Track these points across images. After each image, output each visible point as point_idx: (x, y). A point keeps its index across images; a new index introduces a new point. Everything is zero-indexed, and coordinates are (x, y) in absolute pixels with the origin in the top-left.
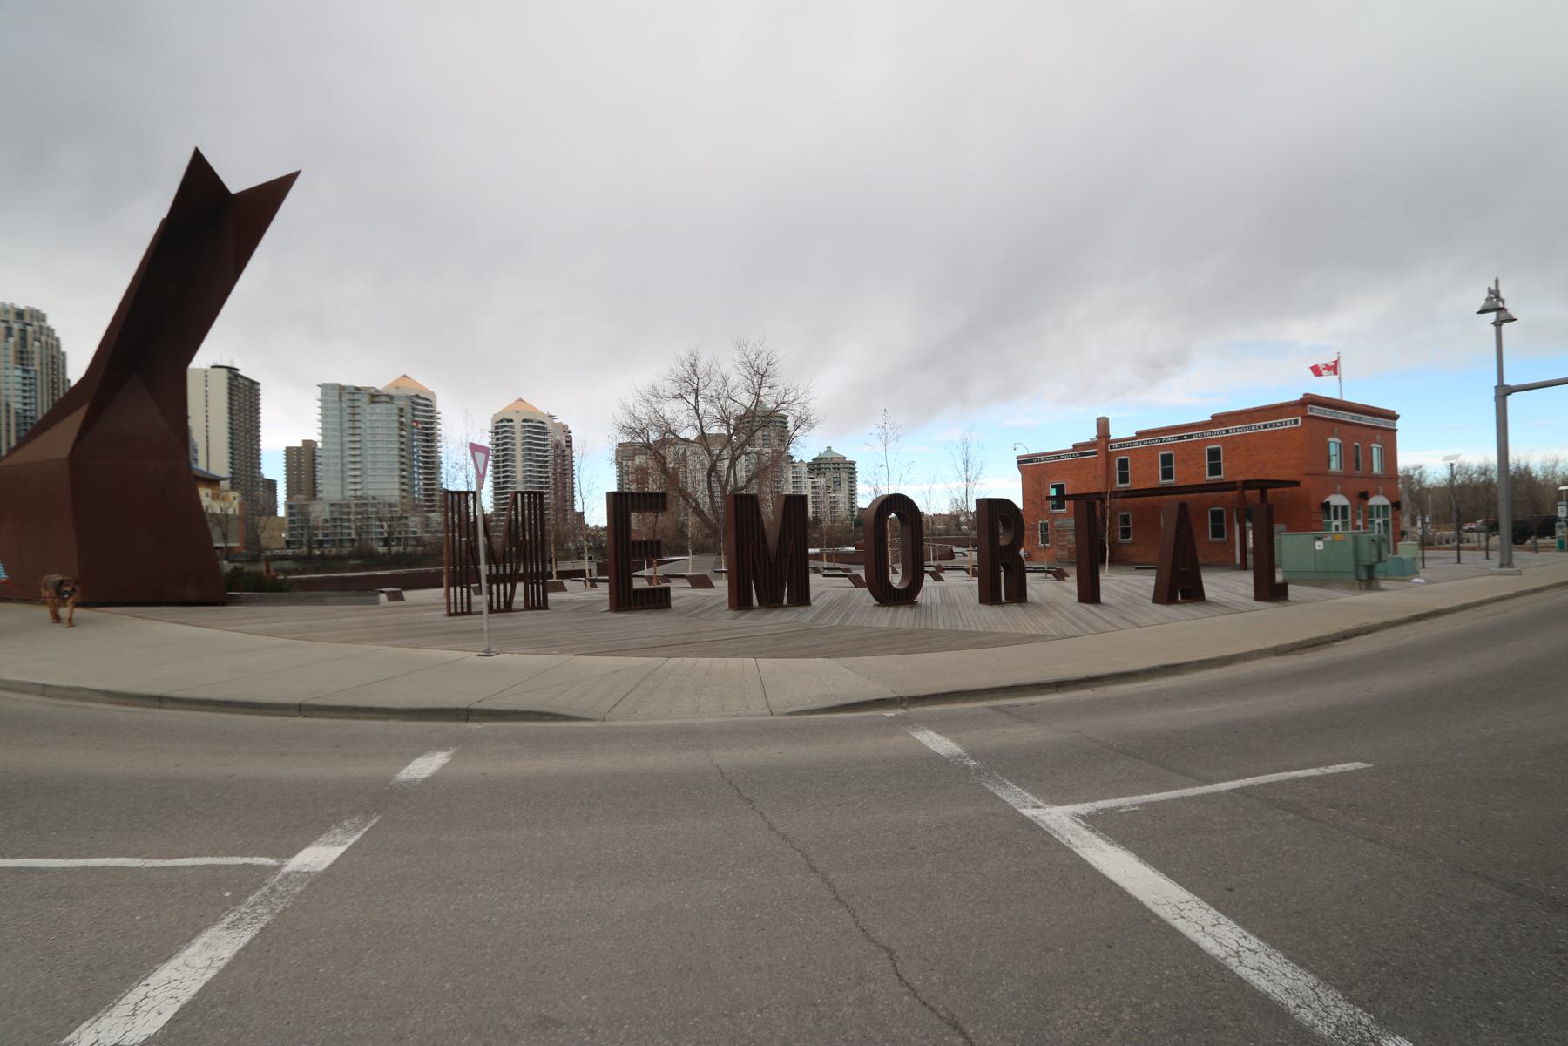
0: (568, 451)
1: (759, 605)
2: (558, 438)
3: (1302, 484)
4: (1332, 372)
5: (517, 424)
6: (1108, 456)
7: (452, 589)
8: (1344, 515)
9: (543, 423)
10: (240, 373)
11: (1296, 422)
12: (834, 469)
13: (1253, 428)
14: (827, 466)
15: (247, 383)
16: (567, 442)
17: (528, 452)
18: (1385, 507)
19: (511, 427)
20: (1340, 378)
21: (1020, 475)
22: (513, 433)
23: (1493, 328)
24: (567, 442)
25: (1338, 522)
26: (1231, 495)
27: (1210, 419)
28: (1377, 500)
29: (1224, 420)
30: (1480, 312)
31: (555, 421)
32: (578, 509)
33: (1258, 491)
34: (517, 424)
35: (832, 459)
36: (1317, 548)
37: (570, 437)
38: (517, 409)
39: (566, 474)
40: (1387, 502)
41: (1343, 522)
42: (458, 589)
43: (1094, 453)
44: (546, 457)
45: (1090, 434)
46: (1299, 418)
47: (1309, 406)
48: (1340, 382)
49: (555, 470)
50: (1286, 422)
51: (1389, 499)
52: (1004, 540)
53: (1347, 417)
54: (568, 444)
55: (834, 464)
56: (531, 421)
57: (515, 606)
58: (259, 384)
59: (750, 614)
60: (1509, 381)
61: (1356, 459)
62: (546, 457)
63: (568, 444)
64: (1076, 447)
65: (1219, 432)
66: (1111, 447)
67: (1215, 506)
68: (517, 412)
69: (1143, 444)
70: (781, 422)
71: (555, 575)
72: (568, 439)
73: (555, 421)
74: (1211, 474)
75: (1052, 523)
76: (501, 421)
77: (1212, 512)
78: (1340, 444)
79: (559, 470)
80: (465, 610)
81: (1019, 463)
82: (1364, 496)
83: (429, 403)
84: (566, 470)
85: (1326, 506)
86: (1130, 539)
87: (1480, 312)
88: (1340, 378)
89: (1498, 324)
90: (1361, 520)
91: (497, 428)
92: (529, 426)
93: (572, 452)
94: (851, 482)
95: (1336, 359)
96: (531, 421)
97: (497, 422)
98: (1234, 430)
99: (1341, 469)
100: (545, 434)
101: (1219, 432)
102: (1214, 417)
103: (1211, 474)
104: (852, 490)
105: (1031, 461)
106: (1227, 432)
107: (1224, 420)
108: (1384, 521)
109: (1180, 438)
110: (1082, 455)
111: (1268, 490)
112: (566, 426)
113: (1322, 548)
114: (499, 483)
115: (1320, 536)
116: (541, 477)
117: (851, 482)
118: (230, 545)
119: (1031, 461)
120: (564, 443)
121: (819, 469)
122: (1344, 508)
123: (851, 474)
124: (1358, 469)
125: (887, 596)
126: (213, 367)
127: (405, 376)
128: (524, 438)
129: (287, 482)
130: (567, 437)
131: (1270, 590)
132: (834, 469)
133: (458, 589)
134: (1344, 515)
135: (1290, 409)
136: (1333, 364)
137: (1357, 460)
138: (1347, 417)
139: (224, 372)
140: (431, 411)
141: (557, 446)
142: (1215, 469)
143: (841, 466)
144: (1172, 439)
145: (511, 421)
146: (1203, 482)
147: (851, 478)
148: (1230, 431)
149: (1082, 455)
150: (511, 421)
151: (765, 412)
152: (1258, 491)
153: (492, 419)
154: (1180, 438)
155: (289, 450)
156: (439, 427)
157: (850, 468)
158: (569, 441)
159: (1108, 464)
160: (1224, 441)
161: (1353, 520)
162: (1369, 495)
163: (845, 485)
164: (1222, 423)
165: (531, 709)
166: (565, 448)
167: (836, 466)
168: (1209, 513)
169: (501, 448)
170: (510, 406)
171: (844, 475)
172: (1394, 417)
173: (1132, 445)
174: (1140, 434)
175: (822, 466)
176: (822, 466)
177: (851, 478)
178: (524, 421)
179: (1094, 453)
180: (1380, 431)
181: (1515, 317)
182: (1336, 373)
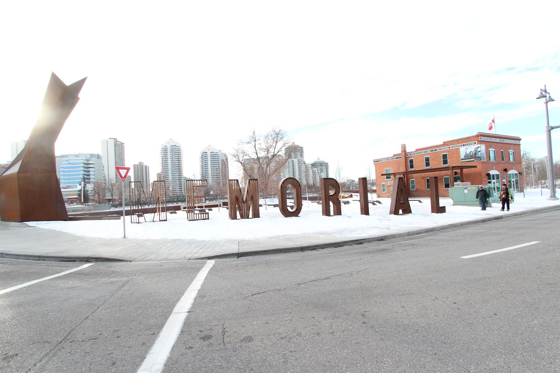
1: (334, 214)
2: (223, 158)
3: (477, 167)
5: (209, 154)
6: (406, 158)
7: (189, 214)
8: (498, 178)
9: (217, 153)
10: (118, 140)
12: (321, 165)
14: (318, 164)
15: (120, 144)
18: (516, 174)
21: (374, 166)
23: (545, 105)
24: (226, 159)
25: (495, 181)
26: (449, 172)
27: (443, 143)
28: (512, 172)
30: (537, 98)
33: (460, 170)
34: (209, 154)
35: (319, 162)
36: (465, 192)
37: (227, 157)
39: (226, 172)
40: (516, 172)
41: (496, 181)
42: (191, 213)
43: (401, 157)
45: (399, 151)
46: (476, 142)
47: (480, 137)
50: (471, 143)
51: (518, 172)
52: (332, 193)
53: (498, 140)
54: (227, 160)
55: (321, 164)
56: (213, 153)
57: (250, 217)
58: (124, 144)
60: (551, 124)
61: (502, 156)
64: (394, 155)
65: (446, 148)
66: (407, 155)
67: (446, 176)
69: (418, 154)
70: (301, 149)
71: (197, 207)
72: (226, 158)
73: (222, 152)
74: (444, 164)
75: (386, 184)
76: (203, 153)
77: (444, 178)
78: (494, 151)
80: (207, 218)
81: (374, 162)
82: (506, 170)
83: (179, 148)
85: (488, 175)
87: (537, 98)
89: (547, 103)
90: (505, 180)
92: (213, 154)
93: (228, 163)
94: (327, 170)
96: (213, 153)
97: (202, 153)
99: (495, 160)
101: (446, 148)
102: (444, 143)
103: (444, 164)
104: (327, 173)
105: (378, 161)
108: (516, 180)
109: (432, 151)
110: (396, 158)
111: (463, 170)
112: (225, 154)
113: (467, 192)
114: (203, 176)
115: (466, 188)
117: (327, 170)
118: (113, 198)
119: (378, 161)
121: (315, 166)
122: (497, 176)
123: (327, 167)
124: (503, 160)
125: (286, 213)
126: (109, 138)
127: (171, 139)
129: (134, 178)
130: (226, 157)
131: (438, 209)
132: (321, 165)
133: (191, 213)
134: (498, 178)
135: (472, 138)
137: (503, 157)
138: (498, 140)
139: (113, 140)
140: (180, 150)
143: (323, 164)
144: (429, 151)
145: (207, 153)
146: (441, 167)
147: (327, 169)
148: (451, 147)
149: (396, 158)
150: (207, 153)
152: (460, 170)
154: (432, 151)
157: (326, 165)
158: (227, 159)
159: (406, 162)
160: (449, 151)
161: (501, 180)
162: (508, 170)
163: (325, 171)
164: (447, 144)
165: (222, 254)
167: (321, 164)
171: (324, 168)
172: (520, 140)
173: (414, 154)
174: (417, 150)
175: (316, 165)
176: (316, 165)
177: (327, 169)
178: (211, 152)
179: (401, 157)
180: (512, 145)
181: (554, 99)
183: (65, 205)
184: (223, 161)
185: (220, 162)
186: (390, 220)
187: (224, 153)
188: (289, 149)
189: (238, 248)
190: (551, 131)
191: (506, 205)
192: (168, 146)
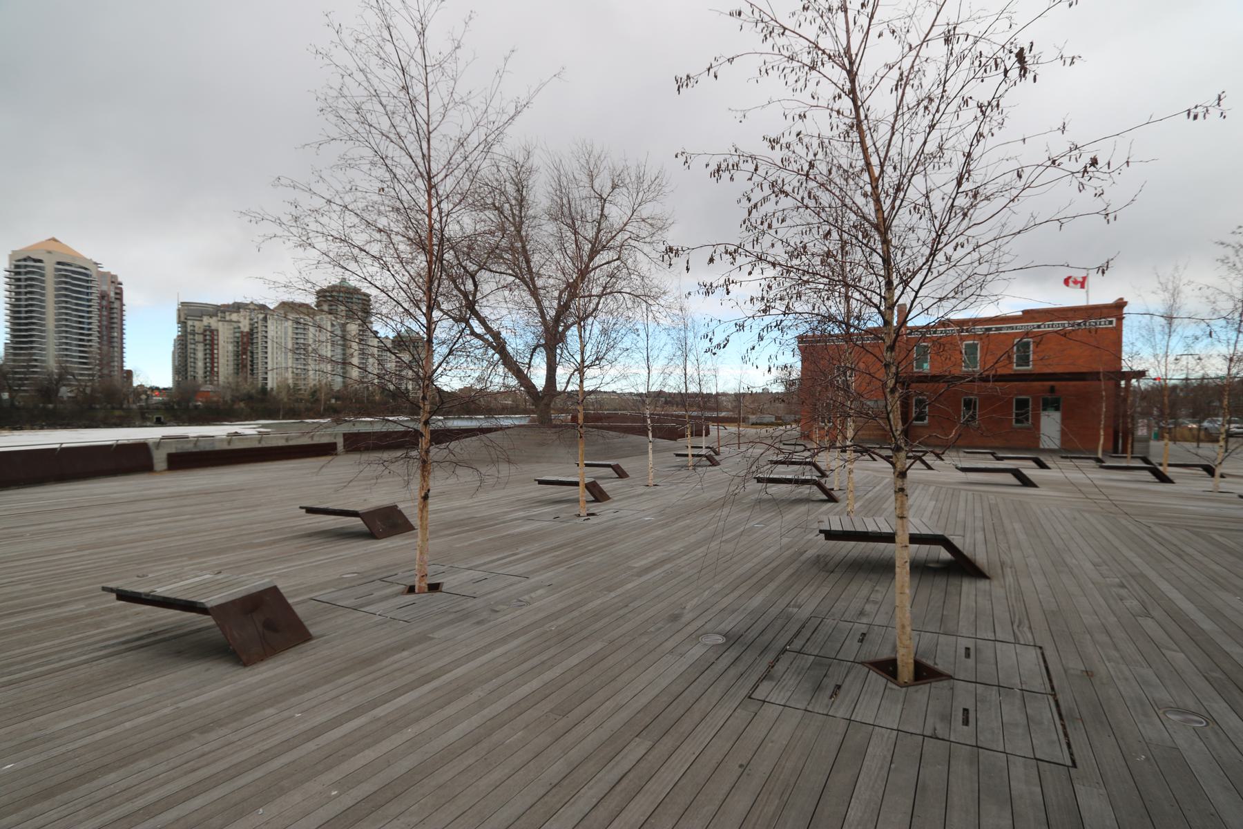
0: (116, 305)
2: (105, 288)
4: (1079, 285)
11: (1111, 322)
13: (1058, 325)
16: (116, 293)
17: (64, 286)
19: (39, 268)
20: (1087, 292)
22: (43, 275)
24: (116, 293)
29: (1036, 315)
31: (100, 269)
32: (1021, 313)
37: (121, 289)
38: (50, 249)
44: (90, 306)
48: (1087, 295)
49: (100, 321)
54: (118, 296)
59: (338, 458)
62: (90, 306)
63: (118, 296)
67: (1021, 395)
68: (49, 252)
72: (118, 291)
73: (100, 269)
76: (25, 260)
79: (105, 323)
84: (113, 323)
86: (926, 422)
88: (1087, 292)
91: (17, 267)
92: (66, 270)
93: (122, 305)
95: (1085, 275)
97: (19, 261)
98: (1047, 327)
100: (87, 281)
102: (1025, 312)
106: (1039, 327)
107: (1036, 315)
112: (115, 277)
116: (80, 322)
120: (112, 294)
128: (57, 320)
130: (117, 288)
135: (1105, 311)
136: (1081, 280)
141: (103, 296)
142: (1024, 360)
145: (40, 261)
151: (348, 288)
153: (11, 256)
155: (826, 539)
156: (8, 324)
158: (119, 294)
166: (113, 300)
168: (1014, 400)
169: (23, 290)
170: (42, 243)
178: (59, 263)
182: (1083, 286)
183: (952, 555)
184: (103, 296)
185: (95, 303)
186: (497, 611)
187: (109, 273)
188: (782, 447)
189: (948, 588)
190: (1039, 651)
191: (356, 523)
192: (46, 269)
